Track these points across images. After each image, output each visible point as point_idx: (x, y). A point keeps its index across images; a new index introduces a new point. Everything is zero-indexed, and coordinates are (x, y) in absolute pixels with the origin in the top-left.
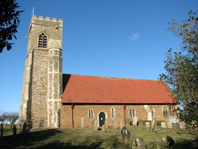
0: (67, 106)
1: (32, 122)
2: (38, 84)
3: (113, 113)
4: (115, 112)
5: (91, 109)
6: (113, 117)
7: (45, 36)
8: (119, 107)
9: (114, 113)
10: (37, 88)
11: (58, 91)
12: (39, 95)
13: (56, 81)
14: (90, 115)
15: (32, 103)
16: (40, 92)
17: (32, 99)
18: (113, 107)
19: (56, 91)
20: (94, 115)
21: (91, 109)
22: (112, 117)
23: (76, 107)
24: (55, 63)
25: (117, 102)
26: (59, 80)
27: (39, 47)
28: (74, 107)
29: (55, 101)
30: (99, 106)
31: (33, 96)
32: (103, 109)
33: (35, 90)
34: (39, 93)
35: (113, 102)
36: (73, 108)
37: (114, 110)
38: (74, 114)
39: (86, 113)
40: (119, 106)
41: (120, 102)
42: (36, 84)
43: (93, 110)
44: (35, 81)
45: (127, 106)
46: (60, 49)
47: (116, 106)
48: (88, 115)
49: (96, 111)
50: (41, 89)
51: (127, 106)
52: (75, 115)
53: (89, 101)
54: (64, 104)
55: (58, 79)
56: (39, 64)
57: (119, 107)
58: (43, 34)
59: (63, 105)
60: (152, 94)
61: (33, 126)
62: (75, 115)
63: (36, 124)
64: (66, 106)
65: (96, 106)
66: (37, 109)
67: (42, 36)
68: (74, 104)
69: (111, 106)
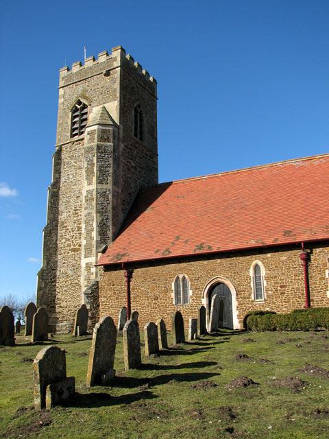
0: (115, 272)
1: (58, 318)
2: (70, 225)
3: (258, 284)
4: (268, 278)
5: (181, 277)
6: (258, 295)
7: (84, 104)
8: (284, 258)
9: (264, 283)
10: (67, 237)
11: (94, 234)
12: (71, 253)
13: (90, 211)
14: (177, 293)
15: (58, 273)
16: (74, 245)
17: (59, 264)
18: (257, 260)
19: (89, 232)
20: (190, 293)
21: (181, 277)
22: (252, 295)
23: (138, 272)
24: (88, 164)
25: (270, 242)
26: (95, 206)
27: (73, 136)
28: (134, 274)
29: (87, 264)
30: (205, 262)
31: (59, 257)
32: (221, 271)
33: (64, 240)
34: (72, 247)
35: (253, 243)
36: (129, 277)
37: (263, 272)
38: (132, 295)
39: (167, 291)
40: (283, 256)
41: (282, 240)
42: (66, 227)
43: (186, 277)
44: (63, 220)
45: (317, 251)
46: (98, 124)
47: (269, 255)
48: (173, 295)
49: (199, 276)
50: (76, 238)
51: (318, 250)
52: (135, 298)
53: (210, 248)
54: (108, 268)
55: (94, 203)
56: (71, 176)
57: (284, 258)
58: (80, 103)
59: (105, 271)
60: (294, 372)
61: (57, 329)
62: (135, 298)
63: (65, 323)
64: (114, 273)
65: (197, 263)
66: (66, 286)
67: (79, 107)
68: (130, 267)
69: (248, 258)
